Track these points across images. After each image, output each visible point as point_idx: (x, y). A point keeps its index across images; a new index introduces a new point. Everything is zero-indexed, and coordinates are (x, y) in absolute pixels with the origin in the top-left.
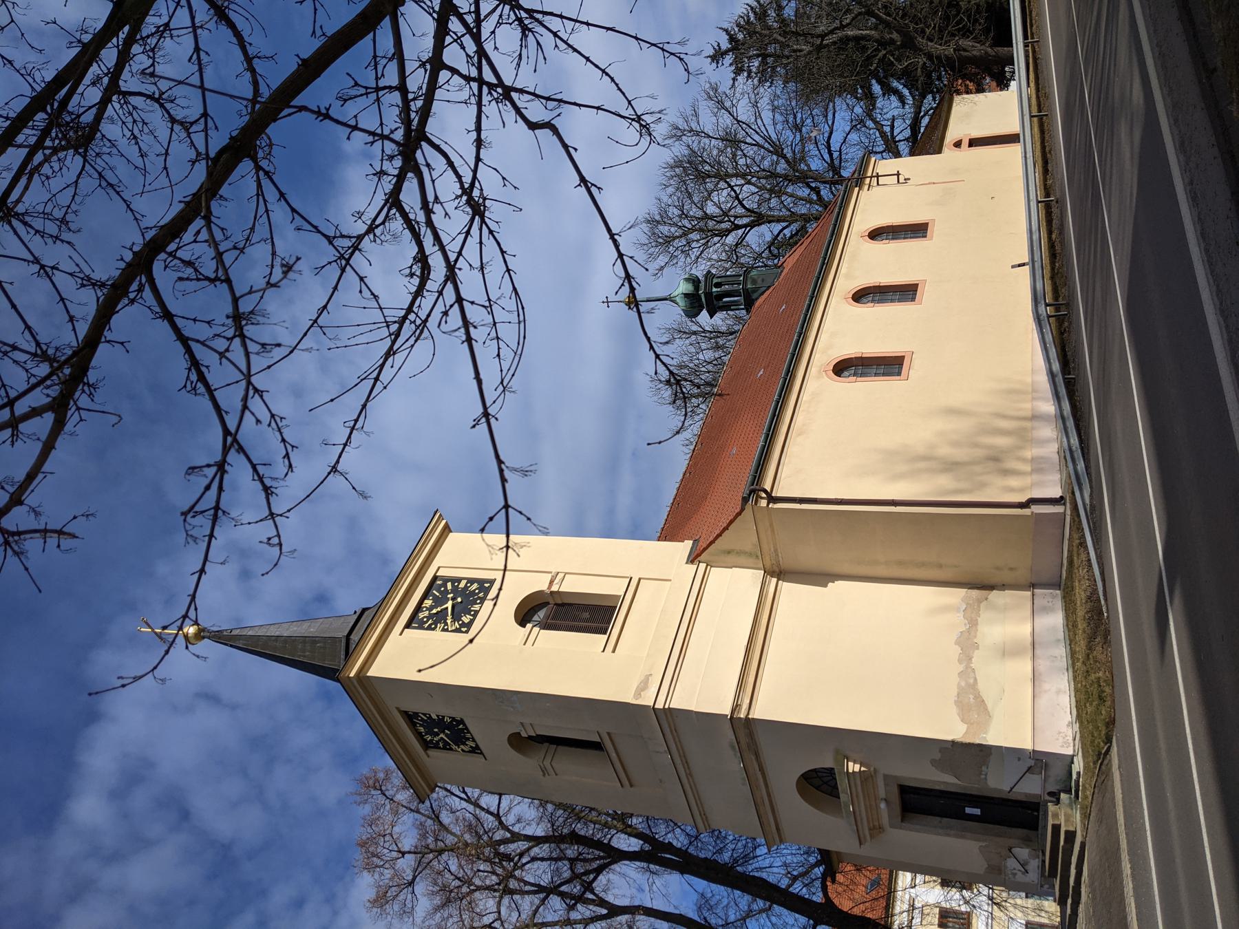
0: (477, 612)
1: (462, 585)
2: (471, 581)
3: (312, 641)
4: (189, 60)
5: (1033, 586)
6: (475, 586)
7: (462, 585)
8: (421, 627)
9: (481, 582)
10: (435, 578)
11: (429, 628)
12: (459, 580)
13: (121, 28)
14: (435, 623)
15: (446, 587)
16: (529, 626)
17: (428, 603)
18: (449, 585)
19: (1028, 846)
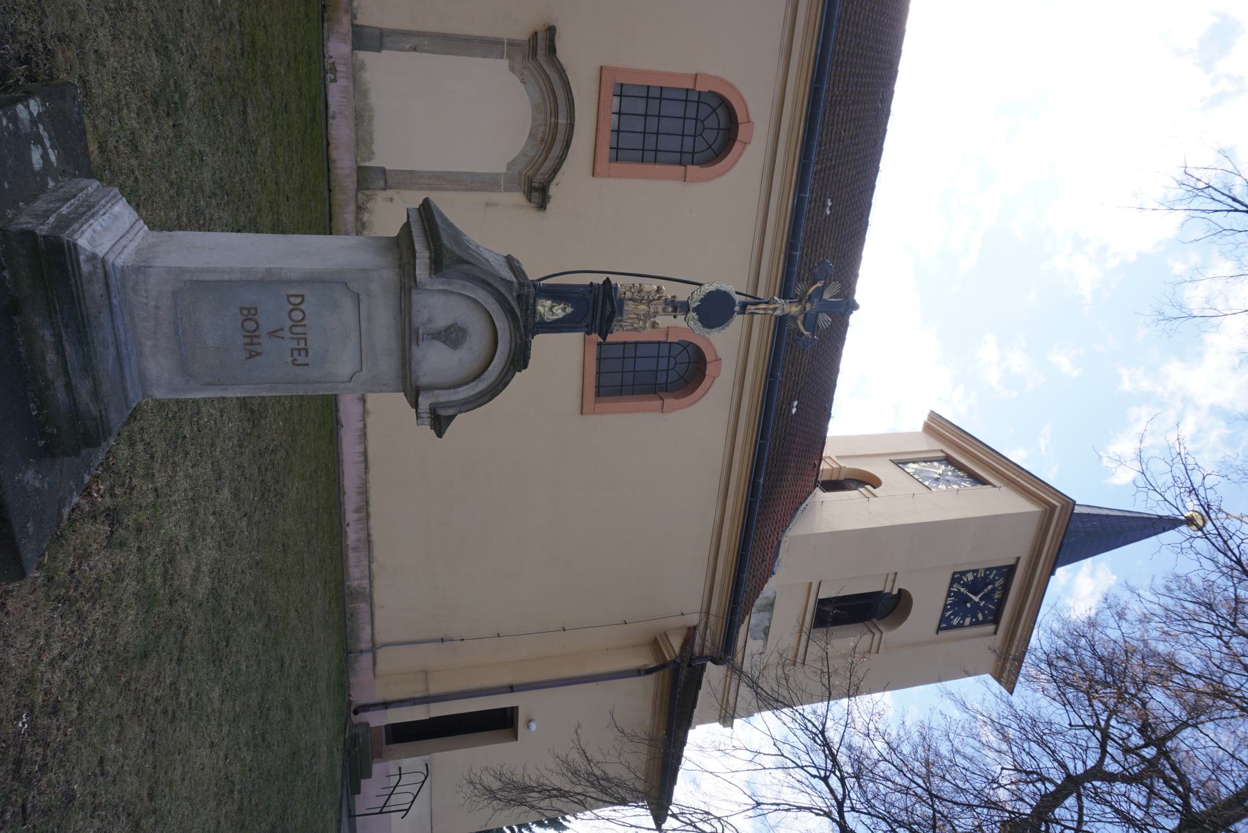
0: (949, 596)
1: (968, 621)
2: (960, 626)
3: (456, 235)
4: (241, 309)
5: (352, 816)
6: (955, 622)
7: (968, 621)
8: (999, 569)
9: (950, 627)
10: (996, 621)
11: (991, 569)
12: (972, 624)
13: (57, 159)
14: (986, 576)
15: (984, 615)
16: (895, 592)
17: (997, 596)
18: (980, 616)
19: (75, 245)
